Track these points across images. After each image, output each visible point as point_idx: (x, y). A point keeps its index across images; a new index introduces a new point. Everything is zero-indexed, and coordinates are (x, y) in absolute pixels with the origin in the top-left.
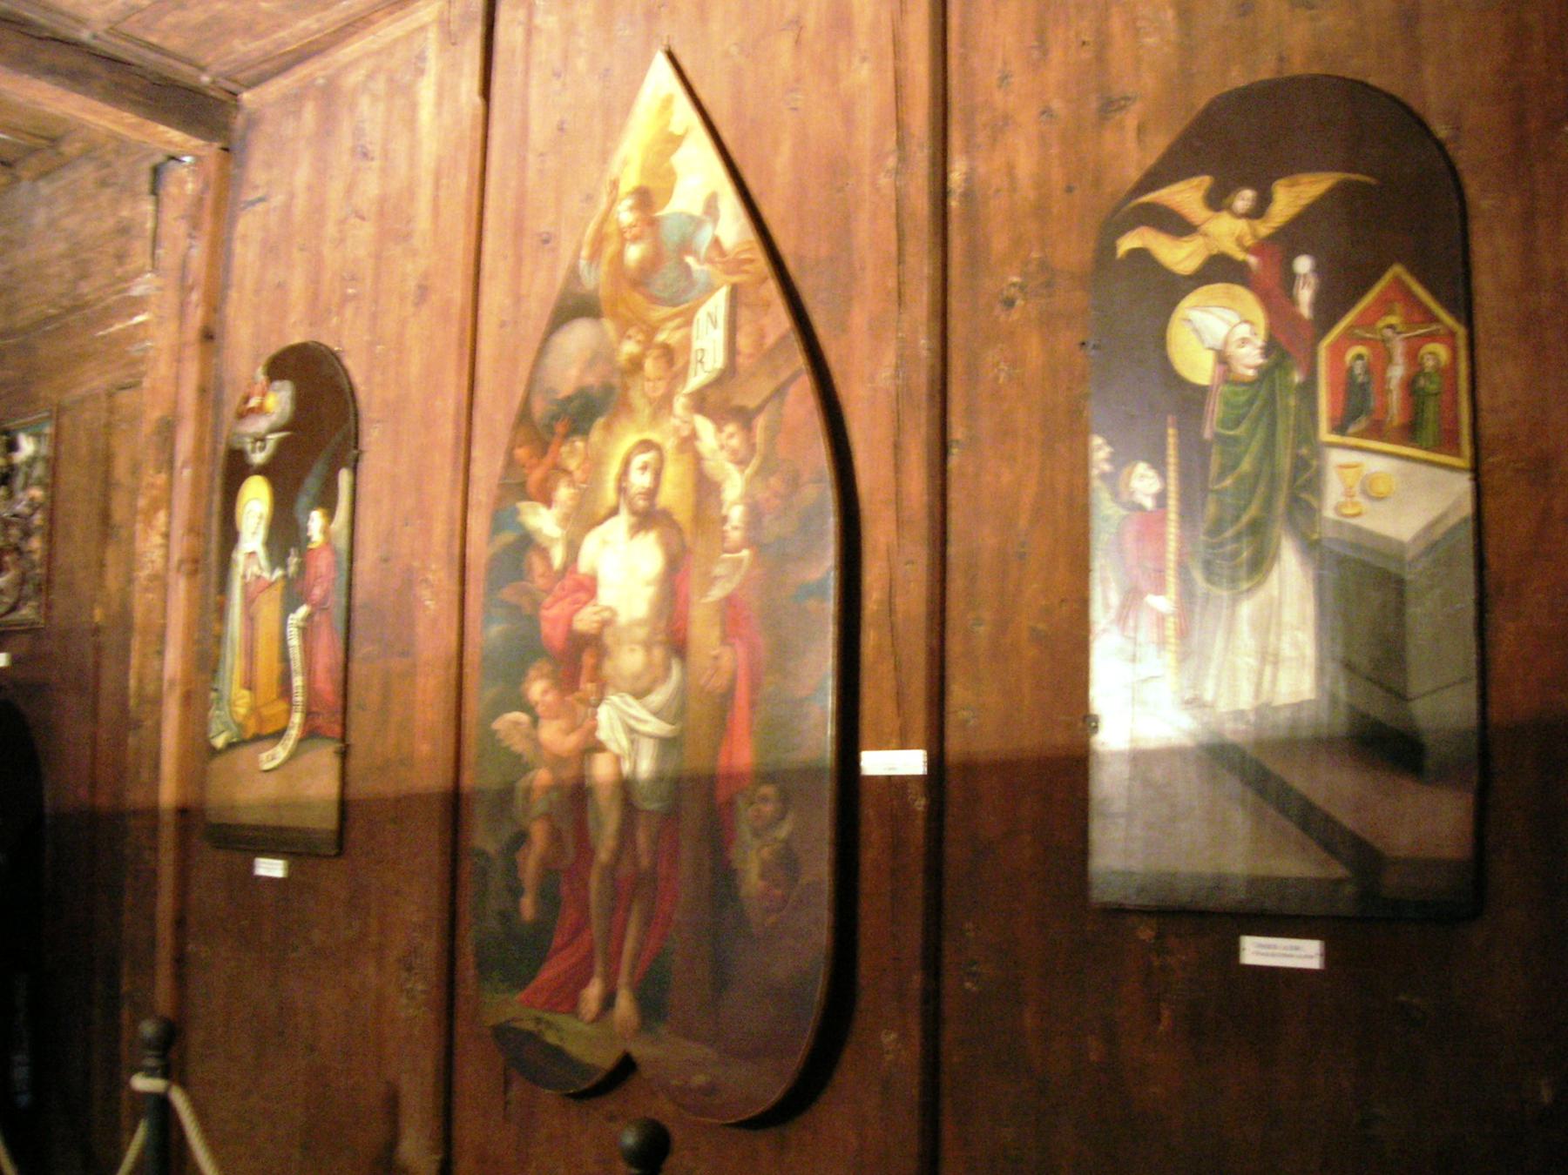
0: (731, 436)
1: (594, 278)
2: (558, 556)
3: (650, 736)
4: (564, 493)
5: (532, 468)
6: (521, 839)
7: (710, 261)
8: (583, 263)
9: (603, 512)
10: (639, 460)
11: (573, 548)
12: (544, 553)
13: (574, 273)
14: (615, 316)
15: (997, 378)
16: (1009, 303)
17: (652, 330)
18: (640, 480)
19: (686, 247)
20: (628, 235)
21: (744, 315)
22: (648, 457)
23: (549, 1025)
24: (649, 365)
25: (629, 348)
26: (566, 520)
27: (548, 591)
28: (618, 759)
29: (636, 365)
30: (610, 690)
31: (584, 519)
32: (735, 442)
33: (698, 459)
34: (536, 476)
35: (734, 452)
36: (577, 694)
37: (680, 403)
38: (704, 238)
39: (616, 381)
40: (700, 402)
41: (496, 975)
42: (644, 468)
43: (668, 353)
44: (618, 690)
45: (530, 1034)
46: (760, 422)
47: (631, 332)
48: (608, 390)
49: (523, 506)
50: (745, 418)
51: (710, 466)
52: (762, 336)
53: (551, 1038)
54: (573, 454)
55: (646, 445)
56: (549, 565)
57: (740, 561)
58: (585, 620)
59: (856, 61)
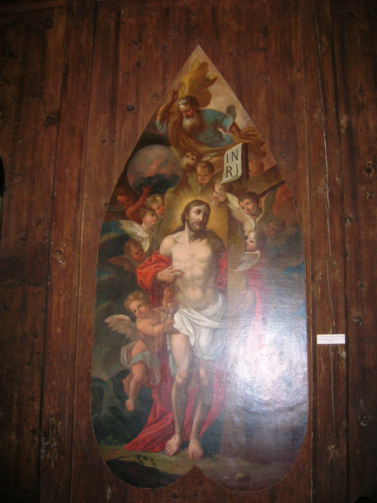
0: (247, 204)
1: (162, 129)
2: (146, 246)
3: (207, 327)
4: (149, 218)
5: (129, 206)
6: (126, 373)
7: (230, 131)
8: (158, 122)
9: (175, 228)
10: (194, 209)
11: (156, 244)
12: (138, 244)
13: (152, 124)
14: (177, 145)
15: (365, 197)
16: (369, 171)
17: (200, 156)
18: (195, 216)
19: (217, 124)
20: (184, 114)
21: (251, 156)
22: (201, 207)
23: (146, 458)
24: (199, 169)
25: (187, 161)
26: (150, 230)
27: (141, 261)
28: (187, 338)
29: (192, 169)
30: (181, 306)
31: (162, 230)
32: (250, 206)
33: (229, 211)
34: (131, 210)
35: (249, 210)
36: (161, 308)
37: (217, 188)
38: (228, 122)
39: (180, 174)
40: (229, 188)
41: (110, 437)
42: (199, 212)
43: (210, 166)
44: (186, 307)
45: (133, 463)
46: (263, 200)
47: (188, 154)
48: (175, 177)
49: (123, 222)
50: (256, 198)
51: (236, 214)
52: (261, 166)
53: (148, 464)
54: (156, 203)
55: (200, 203)
56: (142, 250)
57: (256, 255)
58: (164, 275)
59: (295, 70)
